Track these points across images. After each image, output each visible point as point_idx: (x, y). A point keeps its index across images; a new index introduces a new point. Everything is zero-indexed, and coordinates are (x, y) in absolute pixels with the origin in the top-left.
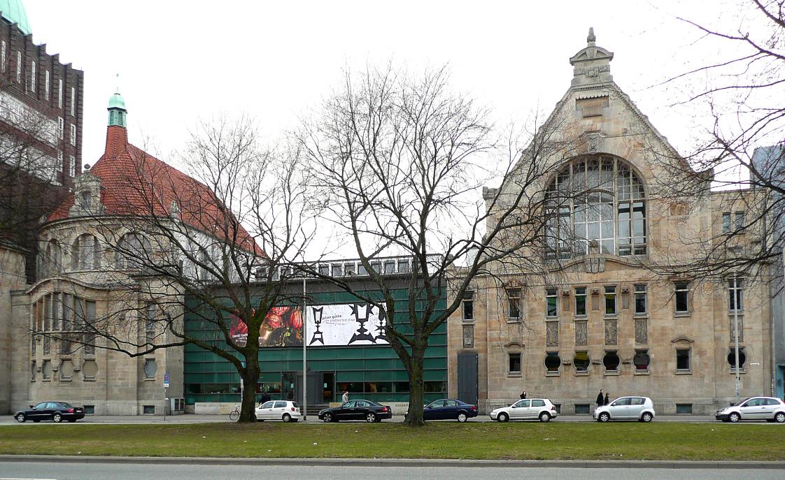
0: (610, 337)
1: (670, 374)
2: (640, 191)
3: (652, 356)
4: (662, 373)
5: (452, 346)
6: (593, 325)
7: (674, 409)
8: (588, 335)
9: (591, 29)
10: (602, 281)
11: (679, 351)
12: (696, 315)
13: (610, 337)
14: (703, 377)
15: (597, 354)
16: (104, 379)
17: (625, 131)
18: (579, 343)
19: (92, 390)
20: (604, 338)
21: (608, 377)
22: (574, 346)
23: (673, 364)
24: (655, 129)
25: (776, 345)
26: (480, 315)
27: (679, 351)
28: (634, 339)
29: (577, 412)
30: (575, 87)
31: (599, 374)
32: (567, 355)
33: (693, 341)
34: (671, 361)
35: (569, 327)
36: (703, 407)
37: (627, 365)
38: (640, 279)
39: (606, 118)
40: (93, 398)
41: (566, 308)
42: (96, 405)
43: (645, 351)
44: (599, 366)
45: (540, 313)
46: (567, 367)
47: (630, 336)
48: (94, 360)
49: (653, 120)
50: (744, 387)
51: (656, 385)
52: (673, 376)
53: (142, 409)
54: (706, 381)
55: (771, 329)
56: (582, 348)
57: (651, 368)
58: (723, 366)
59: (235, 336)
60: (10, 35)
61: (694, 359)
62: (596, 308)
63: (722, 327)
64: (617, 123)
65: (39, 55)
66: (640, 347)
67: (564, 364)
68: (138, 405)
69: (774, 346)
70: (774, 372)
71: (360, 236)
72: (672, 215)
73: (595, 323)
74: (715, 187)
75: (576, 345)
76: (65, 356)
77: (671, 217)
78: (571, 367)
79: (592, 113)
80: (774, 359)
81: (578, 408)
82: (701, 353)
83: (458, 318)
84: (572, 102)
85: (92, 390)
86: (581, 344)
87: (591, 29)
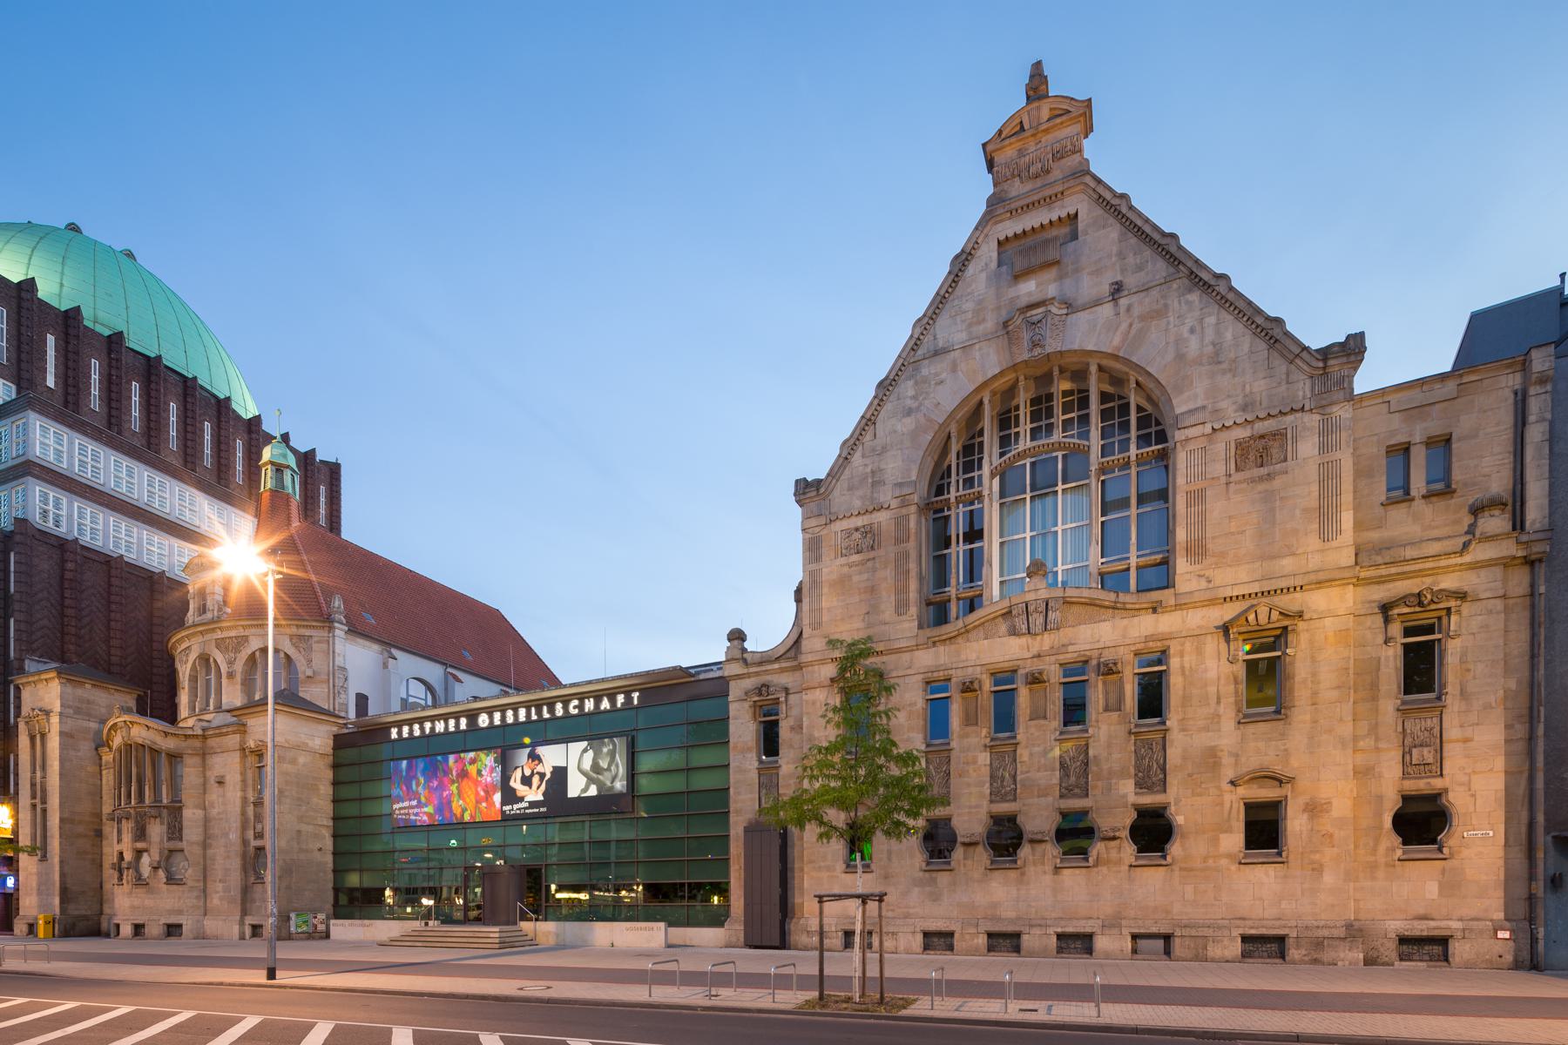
0: (1073, 779)
1: (1224, 862)
2: (1144, 440)
3: (1179, 820)
4: (1205, 859)
5: (738, 812)
6: (1031, 755)
7: (1236, 948)
8: (1018, 778)
9: (1037, 67)
10: (1054, 651)
11: (1250, 807)
12: (1301, 714)
13: (1073, 779)
14: (1318, 869)
15: (1039, 816)
16: (198, 881)
17: (1117, 289)
18: (997, 795)
19: (180, 898)
20: (1056, 780)
21: (1066, 872)
22: (985, 803)
23: (1235, 840)
24: (1197, 261)
25: (1547, 783)
26: (791, 746)
27: (1250, 807)
28: (1132, 782)
29: (991, 949)
30: (997, 206)
31: (1043, 864)
32: (1039, 816)
33: (1291, 780)
34: (1229, 830)
35: (975, 762)
36: (1319, 944)
37: (1113, 843)
38: (1148, 639)
39: (1070, 268)
40: (180, 912)
41: (970, 720)
42: (184, 923)
43: (1011, 819)
44: (1043, 846)
45: (911, 735)
46: (971, 849)
47: (1123, 774)
48: (182, 851)
49: (1192, 243)
50: (1440, 894)
51: (1189, 889)
52: (1234, 867)
53: (248, 931)
54: (1328, 878)
55: (1531, 738)
56: (1004, 808)
57: (1175, 849)
58: (1377, 841)
59: (542, 810)
60: (185, 395)
61: (1295, 824)
62: (1038, 714)
63: (1377, 739)
64: (1097, 272)
65: (250, 432)
66: (1148, 800)
67: (964, 844)
68: (242, 923)
69: (1540, 783)
70: (1540, 855)
71: (92, 306)
72: (1237, 469)
73: (1036, 749)
74: (1366, 380)
75: (991, 802)
76: (140, 845)
77: (1236, 477)
78: (980, 849)
79: (1036, 260)
80: (1540, 818)
81: (994, 942)
82: (1314, 809)
83: (749, 755)
84: (989, 252)
85: (180, 898)
86: (1003, 799)
87: (1037, 67)
